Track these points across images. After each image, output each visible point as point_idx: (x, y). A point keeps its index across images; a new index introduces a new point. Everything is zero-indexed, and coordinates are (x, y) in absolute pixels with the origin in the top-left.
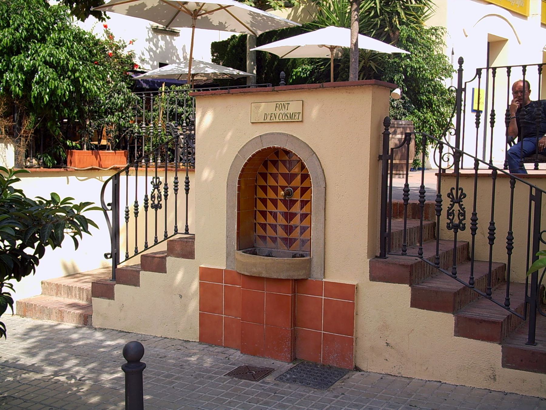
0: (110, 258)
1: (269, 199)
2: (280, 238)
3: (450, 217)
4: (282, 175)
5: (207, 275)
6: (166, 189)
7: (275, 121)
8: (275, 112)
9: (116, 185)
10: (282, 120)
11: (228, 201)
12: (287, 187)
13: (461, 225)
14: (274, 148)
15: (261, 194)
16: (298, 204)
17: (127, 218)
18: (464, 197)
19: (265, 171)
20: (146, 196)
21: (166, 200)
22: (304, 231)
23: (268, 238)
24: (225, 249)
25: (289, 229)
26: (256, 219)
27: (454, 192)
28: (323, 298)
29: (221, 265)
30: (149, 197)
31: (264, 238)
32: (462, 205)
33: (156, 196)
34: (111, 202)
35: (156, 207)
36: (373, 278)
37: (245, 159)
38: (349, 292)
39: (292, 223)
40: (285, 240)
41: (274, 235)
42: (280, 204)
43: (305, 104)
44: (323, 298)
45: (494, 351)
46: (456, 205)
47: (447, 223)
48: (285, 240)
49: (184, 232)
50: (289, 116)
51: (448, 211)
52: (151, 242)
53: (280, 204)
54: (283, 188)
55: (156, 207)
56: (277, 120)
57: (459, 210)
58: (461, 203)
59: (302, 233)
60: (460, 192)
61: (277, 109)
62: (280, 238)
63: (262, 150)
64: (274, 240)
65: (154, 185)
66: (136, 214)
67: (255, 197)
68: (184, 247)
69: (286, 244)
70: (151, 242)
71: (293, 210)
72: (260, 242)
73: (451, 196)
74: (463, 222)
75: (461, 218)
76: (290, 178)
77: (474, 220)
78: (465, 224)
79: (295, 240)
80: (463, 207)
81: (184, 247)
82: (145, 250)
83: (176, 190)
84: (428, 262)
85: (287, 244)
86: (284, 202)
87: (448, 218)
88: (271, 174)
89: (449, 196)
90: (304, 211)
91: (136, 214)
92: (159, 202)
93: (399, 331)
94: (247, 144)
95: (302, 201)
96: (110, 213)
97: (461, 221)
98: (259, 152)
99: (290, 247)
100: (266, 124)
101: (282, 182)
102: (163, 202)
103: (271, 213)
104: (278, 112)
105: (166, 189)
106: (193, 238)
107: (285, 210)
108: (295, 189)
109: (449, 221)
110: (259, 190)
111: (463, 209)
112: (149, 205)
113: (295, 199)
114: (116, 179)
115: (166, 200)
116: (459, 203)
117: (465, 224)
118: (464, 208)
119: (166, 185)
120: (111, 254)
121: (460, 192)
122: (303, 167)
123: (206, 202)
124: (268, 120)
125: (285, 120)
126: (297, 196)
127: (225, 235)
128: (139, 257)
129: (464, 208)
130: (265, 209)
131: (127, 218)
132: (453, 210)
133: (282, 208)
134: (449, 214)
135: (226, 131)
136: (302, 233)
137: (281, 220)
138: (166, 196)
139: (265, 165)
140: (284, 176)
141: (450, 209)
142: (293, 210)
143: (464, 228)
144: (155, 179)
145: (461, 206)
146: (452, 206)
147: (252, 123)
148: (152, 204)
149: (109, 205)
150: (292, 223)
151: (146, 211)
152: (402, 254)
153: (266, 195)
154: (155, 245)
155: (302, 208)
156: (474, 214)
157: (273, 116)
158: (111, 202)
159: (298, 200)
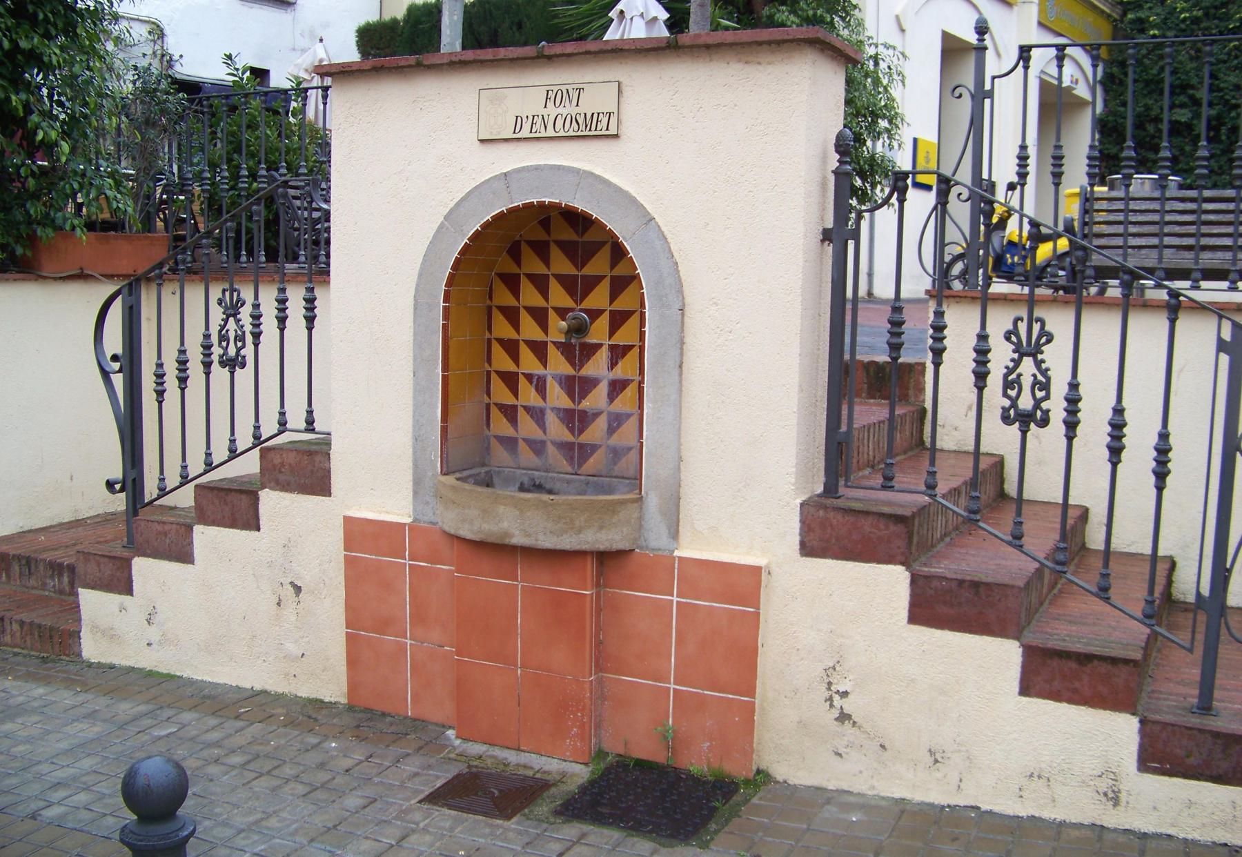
0: (122, 490)
1: (527, 342)
2: (553, 443)
3: (1009, 392)
4: (561, 279)
5: (360, 535)
6: (256, 317)
7: (543, 134)
8: (545, 112)
9: (131, 308)
10: (562, 133)
11: (419, 345)
12: (572, 310)
13: (1039, 413)
14: (541, 205)
15: (503, 329)
16: (603, 355)
17: (160, 394)
18: (1049, 341)
19: (515, 270)
20: (207, 337)
21: (256, 345)
22: (619, 426)
23: (521, 444)
24: (411, 471)
25: (577, 420)
26: (491, 298)
27: (1022, 327)
28: (675, 599)
29: (395, 507)
30: (215, 339)
31: (510, 443)
32: (1043, 361)
33: (232, 335)
34: (119, 350)
35: (233, 364)
36: (807, 549)
37: (464, 235)
38: (743, 585)
39: (586, 404)
40: (566, 448)
41: (536, 433)
42: (553, 354)
43: (624, 89)
44: (675, 599)
45: (1119, 732)
46: (1028, 363)
47: (1003, 408)
48: (566, 448)
49: (303, 425)
50: (581, 120)
51: (1006, 376)
52: (220, 454)
53: (553, 354)
54: (562, 313)
55: (233, 364)
56: (550, 133)
57: (1034, 376)
58: (1040, 357)
59: (611, 430)
60: (1036, 327)
61: (550, 104)
62: (553, 443)
63: (511, 211)
64: (538, 447)
65: (226, 308)
66: (183, 380)
67: (487, 335)
68: (306, 468)
69: (570, 460)
70: (220, 454)
71: (589, 370)
72: (500, 455)
73: (1014, 339)
74: (1044, 405)
75: (1039, 394)
76: (579, 288)
77: (1073, 401)
78: (1048, 411)
79: (594, 448)
80: (1044, 366)
81: (306, 468)
82: (206, 472)
83: (282, 321)
84: (944, 502)
85: (572, 458)
86: (566, 349)
87: (1005, 395)
88: (529, 276)
89: (1008, 339)
90: (619, 373)
91: (183, 380)
92: (239, 350)
93: (867, 682)
94: (468, 194)
95: (613, 348)
96: (118, 380)
97: (1037, 403)
98: (500, 217)
99: (580, 466)
100: (521, 144)
101: (559, 296)
102: (248, 351)
103: (529, 377)
104: (552, 111)
105: (256, 317)
106: (327, 443)
107: (568, 370)
108: (595, 314)
109: (1007, 403)
110: (498, 352)
111: (1044, 372)
112: (215, 358)
113: (595, 341)
114: (130, 294)
115: (256, 345)
116: (1034, 356)
117: (1048, 411)
118: (1047, 370)
119: (256, 306)
120: (124, 482)
121: (1036, 327)
122: (618, 252)
123: (364, 352)
124: (525, 133)
125: (571, 133)
126: (599, 332)
127: (410, 435)
128: (190, 488)
129: (1047, 370)
130: (511, 367)
131: (160, 394)
132: (1020, 375)
133: (558, 365)
134: (1007, 385)
135: (411, 175)
136: (611, 430)
137: (558, 397)
138: (257, 336)
139: (515, 252)
140: (568, 283)
141: (1010, 371)
142: (589, 370)
143: (1044, 422)
144: (227, 294)
145: (1038, 364)
146: (1017, 363)
147: (482, 141)
148: (221, 357)
149: (115, 358)
150: (586, 404)
151: (208, 374)
152: (884, 487)
153: (518, 331)
154: (230, 459)
155: (613, 365)
156: (1074, 386)
157: (538, 121)
158: (119, 350)
159: (600, 345)
